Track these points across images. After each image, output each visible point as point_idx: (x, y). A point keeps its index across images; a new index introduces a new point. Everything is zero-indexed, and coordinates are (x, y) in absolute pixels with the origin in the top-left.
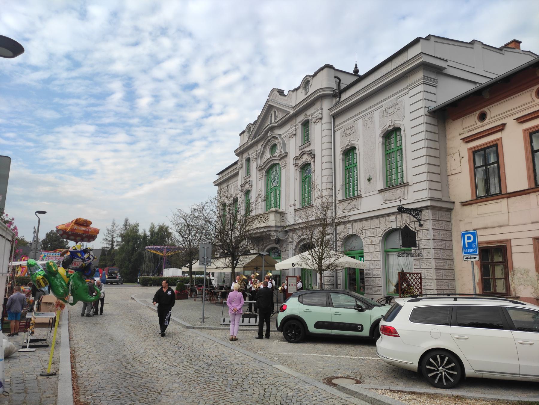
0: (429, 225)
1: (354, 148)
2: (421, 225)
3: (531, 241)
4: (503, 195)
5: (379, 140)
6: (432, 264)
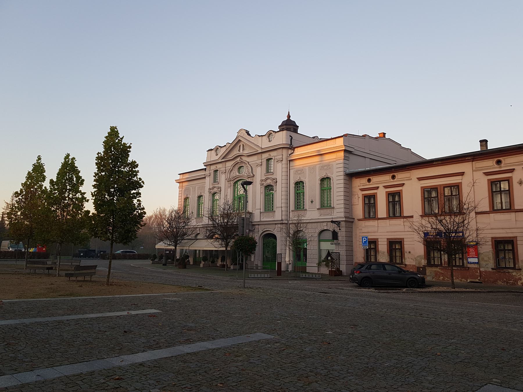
0: (343, 229)
1: (328, 178)
2: (340, 229)
3: (386, 240)
4: (375, 218)
5: (197, 199)
6: (344, 248)
